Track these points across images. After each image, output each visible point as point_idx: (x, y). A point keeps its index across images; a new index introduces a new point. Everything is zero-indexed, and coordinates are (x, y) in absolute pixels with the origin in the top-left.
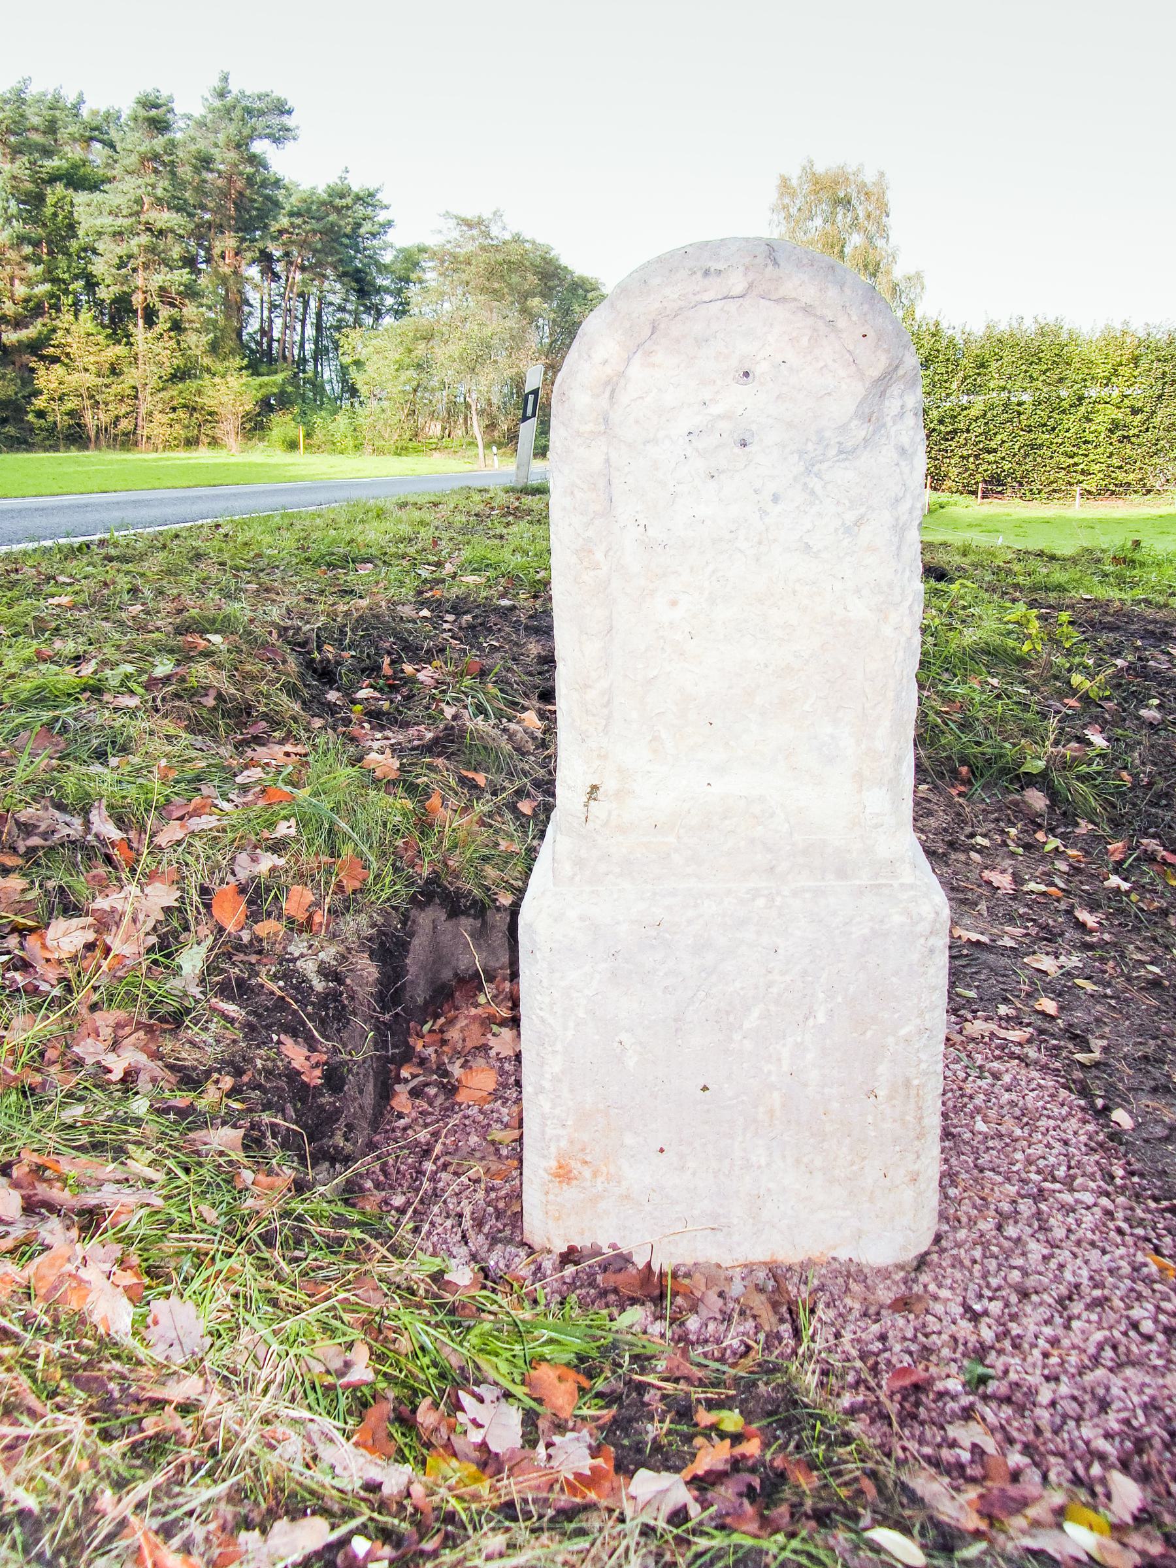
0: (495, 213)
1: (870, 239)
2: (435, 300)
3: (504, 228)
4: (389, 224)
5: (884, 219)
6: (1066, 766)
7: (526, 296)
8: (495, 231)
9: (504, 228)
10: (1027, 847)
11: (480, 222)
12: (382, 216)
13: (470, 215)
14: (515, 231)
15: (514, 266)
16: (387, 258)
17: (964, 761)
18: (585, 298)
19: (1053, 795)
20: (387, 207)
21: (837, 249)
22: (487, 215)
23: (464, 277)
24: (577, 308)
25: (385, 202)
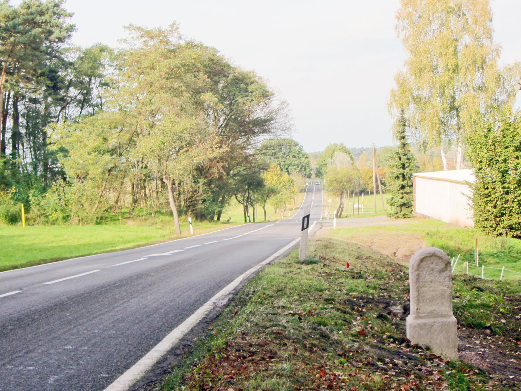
0: (172, 25)
1: (477, 39)
2: (117, 96)
3: (180, 38)
4: (71, 29)
5: (489, 23)
6: (495, 325)
7: (198, 92)
8: (173, 39)
9: (180, 38)
10: (484, 338)
11: (160, 33)
12: (67, 22)
13: (151, 26)
14: (188, 39)
15: (189, 68)
16: (71, 57)
17: (473, 324)
18: (246, 91)
19: (491, 330)
20: (71, 15)
21: (451, 50)
22: (165, 27)
23: (149, 79)
24: (240, 100)
25: (69, 11)
